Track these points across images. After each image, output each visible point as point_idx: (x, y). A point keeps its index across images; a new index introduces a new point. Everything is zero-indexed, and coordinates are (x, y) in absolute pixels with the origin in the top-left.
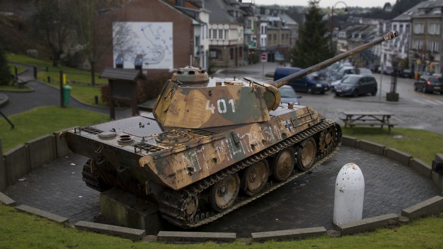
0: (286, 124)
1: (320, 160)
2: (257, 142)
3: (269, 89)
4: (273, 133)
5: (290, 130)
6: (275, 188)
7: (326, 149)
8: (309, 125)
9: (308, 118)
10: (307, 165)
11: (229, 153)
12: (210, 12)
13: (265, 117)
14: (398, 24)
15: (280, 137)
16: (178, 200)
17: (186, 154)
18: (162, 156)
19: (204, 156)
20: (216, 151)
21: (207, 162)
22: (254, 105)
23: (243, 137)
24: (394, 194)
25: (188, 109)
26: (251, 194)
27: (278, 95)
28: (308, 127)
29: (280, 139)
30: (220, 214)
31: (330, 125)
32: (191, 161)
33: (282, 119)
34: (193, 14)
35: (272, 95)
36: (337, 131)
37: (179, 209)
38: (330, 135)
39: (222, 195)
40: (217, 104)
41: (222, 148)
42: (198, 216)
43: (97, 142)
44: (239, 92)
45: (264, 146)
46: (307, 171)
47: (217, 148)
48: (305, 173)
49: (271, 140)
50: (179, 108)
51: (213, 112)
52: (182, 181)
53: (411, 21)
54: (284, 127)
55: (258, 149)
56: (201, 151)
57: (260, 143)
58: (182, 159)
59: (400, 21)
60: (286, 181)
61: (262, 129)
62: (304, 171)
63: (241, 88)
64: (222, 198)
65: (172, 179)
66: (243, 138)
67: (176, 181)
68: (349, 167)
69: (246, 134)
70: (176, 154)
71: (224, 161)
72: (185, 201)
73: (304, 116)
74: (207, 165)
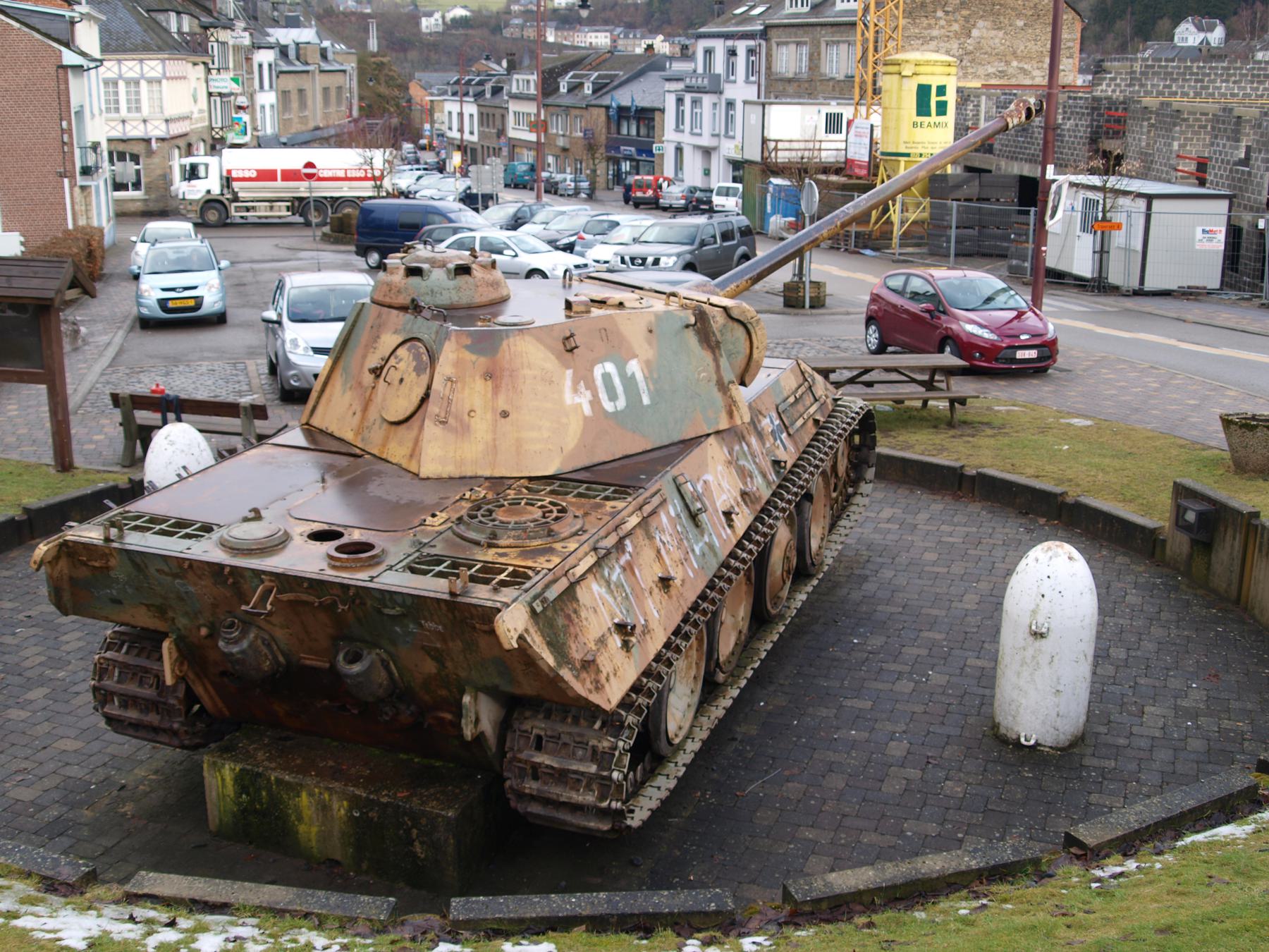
2: (733, 502)
3: (735, 314)
8: (816, 422)
12: (104, 18)
13: (735, 413)
14: (719, 46)
16: (590, 743)
17: (598, 576)
18: (552, 594)
22: (699, 374)
25: (506, 408)
27: (759, 333)
28: (814, 431)
32: (615, 599)
34: (58, 29)
35: (740, 332)
37: (605, 773)
40: (593, 381)
43: (219, 568)
47: (658, 538)
50: (467, 408)
51: (587, 410)
53: (764, 34)
56: (627, 557)
58: (595, 599)
59: (727, 36)
63: (653, 318)
67: (603, 678)
68: (1057, 555)
70: (578, 582)
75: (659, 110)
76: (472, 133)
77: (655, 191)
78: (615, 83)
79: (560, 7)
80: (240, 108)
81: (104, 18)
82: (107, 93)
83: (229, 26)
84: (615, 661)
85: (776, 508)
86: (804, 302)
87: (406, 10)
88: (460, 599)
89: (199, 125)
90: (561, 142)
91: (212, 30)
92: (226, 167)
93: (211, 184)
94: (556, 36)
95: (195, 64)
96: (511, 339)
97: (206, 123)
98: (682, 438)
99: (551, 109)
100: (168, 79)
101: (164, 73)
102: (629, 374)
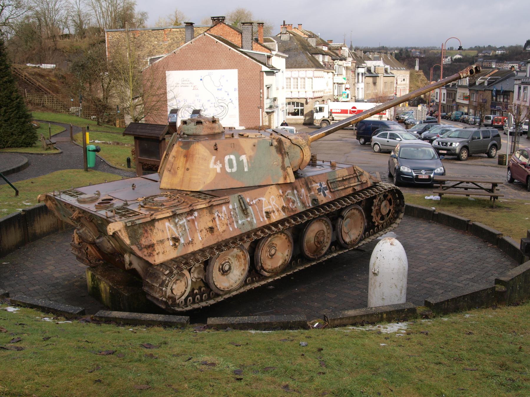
0: (319, 187)
1: (372, 235)
2: (274, 209)
3: (294, 142)
4: (299, 198)
5: (325, 195)
6: (301, 268)
7: (382, 222)
8: (354, 189)
9: (353, 180)
10: (351, 241)
11: (233, 222)
13: (288, 178)
15: (309, 204)
17: (171, 221)
18: (138, 222)
19: (196, 223)
20: (214, 219)
21: (201, 231)
22: (274, 163)
23: (254, 202)
24: (464, 282)
26: (266, 274)
28: (351, 192)
29: (309, 206)
30: (221, 297)
31: (386, 189)
32: (177, 229)
33: (314, 181)
34: (265, 61)
36: (398, 198)
38: (388, 202)
39: (225, 273)
40: (224, 161)
41: (223, 215)
42: (190, 298)
44: (254, 146)
45: (284, 214)
46: (351, 248)
47: (216, 214)
48: (347, 250)
49: (296, 207)
51: (219, 170)
52: (163, 253)
54: (317, 192)
55: (274, 218)
56: (193, 217)
57: (278, 211)
58: (165, 228)
60: (319, 259)
61: (283, 192)
62: (346, 248)
64: (225, 277)
65: (150, 251)
66: (254, 203)
67: (155, 253)
69: (260, 199)
70: (158, 220)
71: (224, 231)
72: (168, 279)
73: (348, 177)
74: (199, 236)
75: (512, 92)
76: (444, 100)
77: (502, 123)
78: (497, 81)
79: (498, 54)
80: (346, 89)
81: (287, 56)
82: (287, 82)
83: (343, 59)
84: (165, 249)
85: (307, 216)
86: (506, 163)
87: (437, 56)
88: (109, 219)
89: (329, 94)
90: (474, 104)
91: (336, 61)
92: (330, 108)
93: (325, 114)
94: (496, 65)
95: (328, 72)
96: (194, 144)
97: (332, 94)
98: (260, 185)
99: (472, 91)
100: (315, 77)
101: (314, 75)
102: (241, 159)
